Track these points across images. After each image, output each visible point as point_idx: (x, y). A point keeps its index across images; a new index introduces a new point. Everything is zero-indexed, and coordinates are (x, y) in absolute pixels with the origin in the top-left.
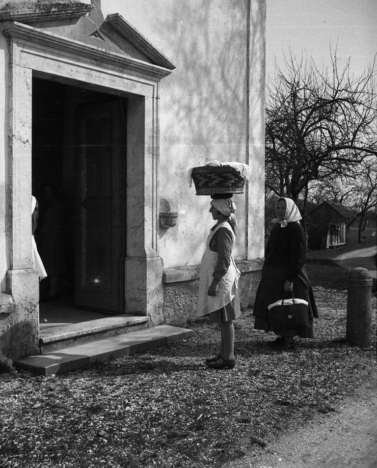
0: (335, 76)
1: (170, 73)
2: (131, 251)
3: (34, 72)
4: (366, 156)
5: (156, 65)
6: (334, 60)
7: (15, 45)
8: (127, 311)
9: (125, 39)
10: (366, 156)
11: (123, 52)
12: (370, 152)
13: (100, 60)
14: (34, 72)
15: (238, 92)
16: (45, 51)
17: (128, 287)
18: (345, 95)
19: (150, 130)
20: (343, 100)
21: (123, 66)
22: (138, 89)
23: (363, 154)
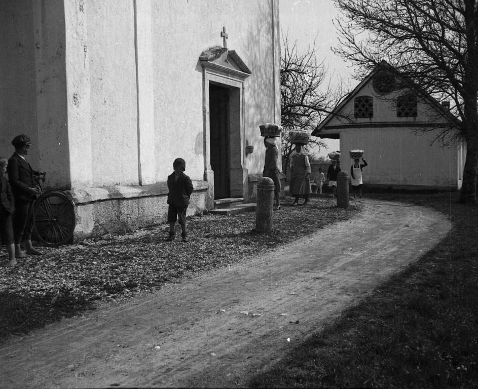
0: (287, 53)
1: (249, 76)
2: (232, 166)
3: (210, 81)
4: (312, 112)
5: (243, 71)
6: (285, 41)
7: (206, 71)
8: (231, 196)
9: (234, 61)
10: (312, 112)
11: (232, 66)
12: (315, 109)
13: (227, 72)
14: (210, 81)
15: (444, 235)
16: (212, 71)
17: (231, 184)
18: (293, 67)
19: (326, 144)
20: (292, 70)
21: (233, 74)
22: (239, 85)
23: (310, 110)
